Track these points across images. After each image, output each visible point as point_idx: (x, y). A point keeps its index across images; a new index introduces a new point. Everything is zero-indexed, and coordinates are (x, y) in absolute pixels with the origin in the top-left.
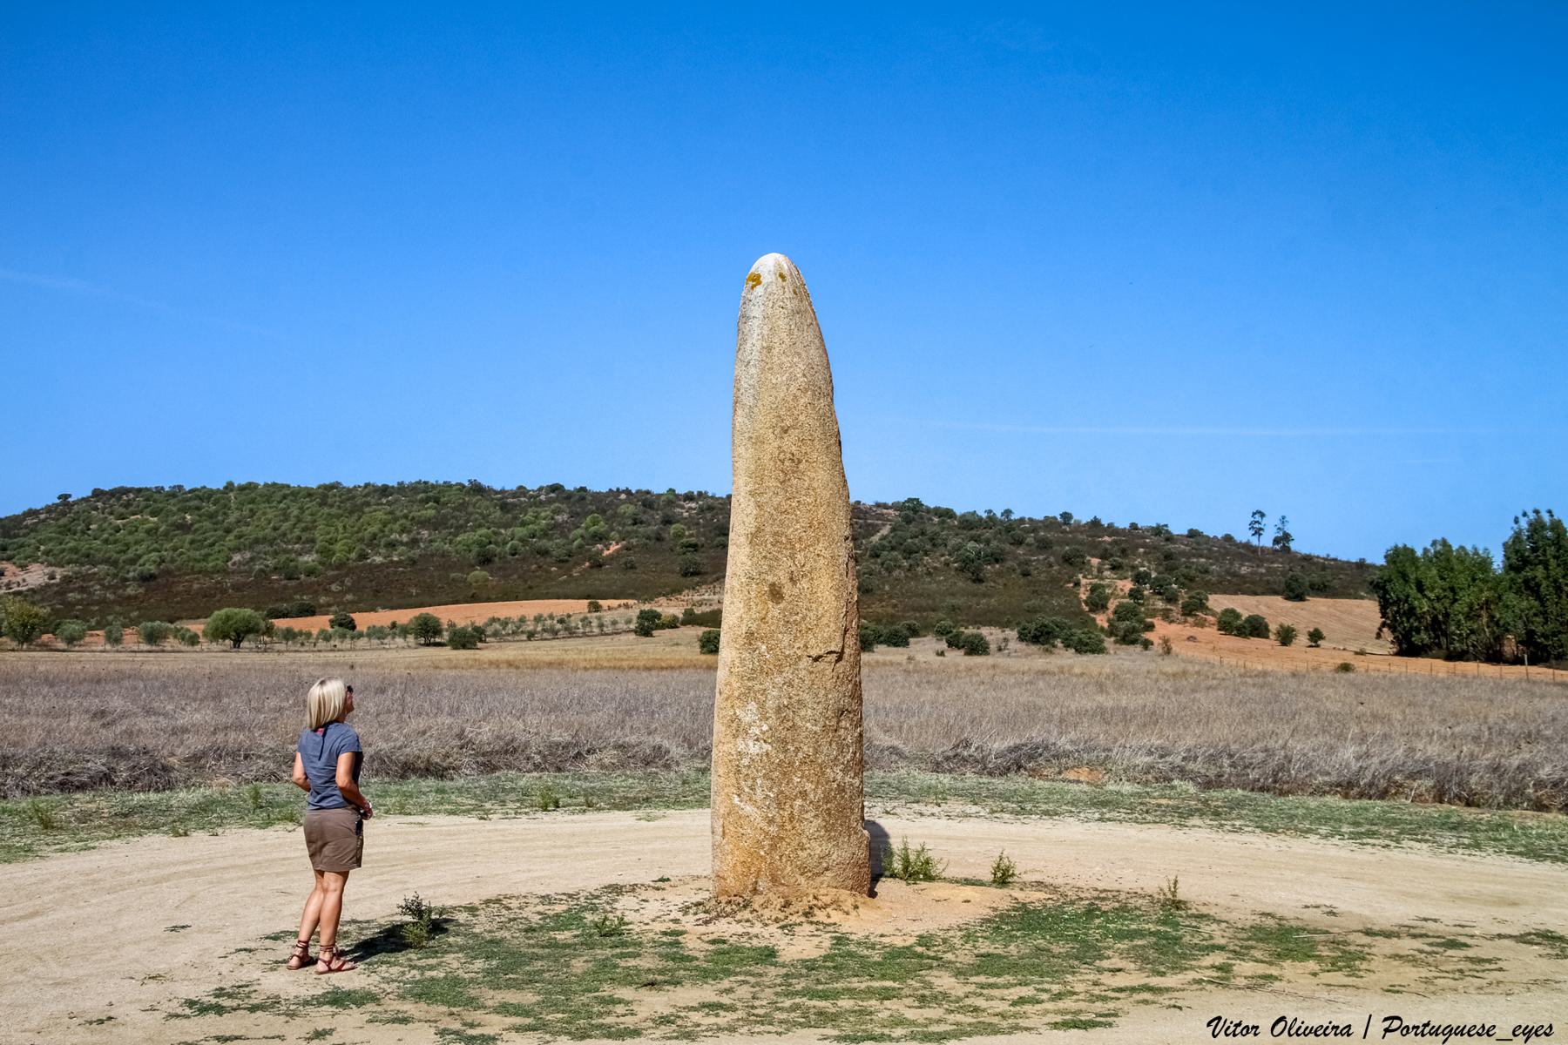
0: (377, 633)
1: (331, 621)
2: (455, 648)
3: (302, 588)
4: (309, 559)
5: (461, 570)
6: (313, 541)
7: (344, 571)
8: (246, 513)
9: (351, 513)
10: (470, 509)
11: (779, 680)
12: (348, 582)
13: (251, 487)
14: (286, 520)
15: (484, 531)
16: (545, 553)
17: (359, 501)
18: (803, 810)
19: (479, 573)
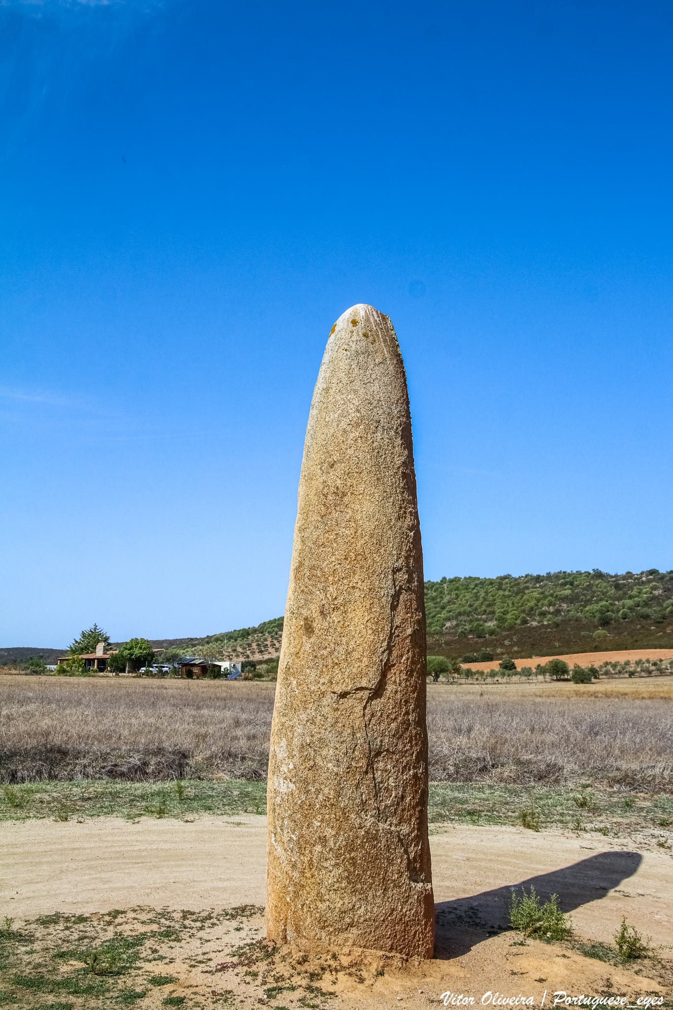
0: (527, 672)
1: (500, 664)
2: (577, 683)
3: (486, 644)
4: (491, 624)
5: (589, 630)
6: (493, 613)
7: (513, 632)
8: (454, 596)
9: (517, 594)
10: (594, 588)
11: (304, 717)
12: (515, 639)
13: (456, 580)
14: (477, 600)
15: (604, 603)
16: (646, 617)
17: (522, 586)
18: (323, 858)
19: (601, 631)
